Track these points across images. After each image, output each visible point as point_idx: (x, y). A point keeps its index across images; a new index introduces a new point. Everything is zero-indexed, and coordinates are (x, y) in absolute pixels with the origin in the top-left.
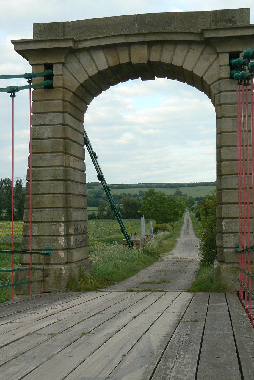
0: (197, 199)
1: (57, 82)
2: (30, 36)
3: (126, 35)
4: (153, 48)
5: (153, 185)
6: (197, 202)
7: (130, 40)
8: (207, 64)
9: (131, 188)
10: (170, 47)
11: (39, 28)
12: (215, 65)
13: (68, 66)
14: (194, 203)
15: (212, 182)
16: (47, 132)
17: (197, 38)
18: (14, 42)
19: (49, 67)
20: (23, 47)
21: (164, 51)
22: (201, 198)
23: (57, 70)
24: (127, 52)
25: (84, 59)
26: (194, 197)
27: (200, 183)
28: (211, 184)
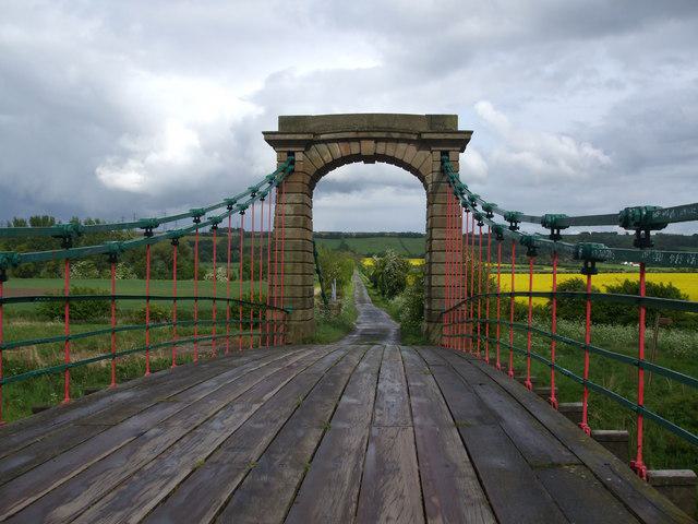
2: (275, 128)
7: (361, 135)
18: (264, 133)
20: (272, 137)
23: (299, 156)
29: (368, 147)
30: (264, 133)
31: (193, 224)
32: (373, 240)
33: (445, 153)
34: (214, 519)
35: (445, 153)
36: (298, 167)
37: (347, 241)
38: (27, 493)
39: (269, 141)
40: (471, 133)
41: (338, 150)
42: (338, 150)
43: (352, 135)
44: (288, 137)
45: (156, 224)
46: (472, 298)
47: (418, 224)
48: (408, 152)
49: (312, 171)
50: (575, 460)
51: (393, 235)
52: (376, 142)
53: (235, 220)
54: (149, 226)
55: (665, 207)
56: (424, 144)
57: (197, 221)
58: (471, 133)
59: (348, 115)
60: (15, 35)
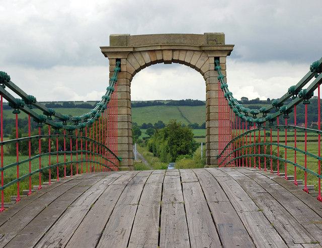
0: (144, 126)
1: (124, 69)
2: (108, 45)
3: (161, 46)
4: (175, 52)
5: (76, 104)
6: (145, 131)
7: (163, 48)
8: (203, 62)
9: (73, 107)
10: (184, 52)
11: (113, 39)
12: (207, 62)
13: (129, 60)
14: (140, 134)
15: (167, 101)
16: (124, 89)
17: (198, 49)
18: (101, 48)
19: (118, 60)
20: (106, 50)
21: (181, 54)
22: (150, 125)
23: (123, 62)
24: (161, 53)
25: (138, 56)
26: (140, 124)
27: (148, 101)
28: (165, 103)
29: (168, 56)
32: (149, 108)
33: (217, 58)
34: (43, 246)
35: (217, 58)
39: (103, 53)
40: (234, 46)
41: (147, 58)
44: (116, 50)
46: (193, 145)
48: (195, 59)
50: (266, 192)
51: (172, 103)
55: (107, 84)
56: (202, 50)
58: (234, 46)
59: (143, 35)
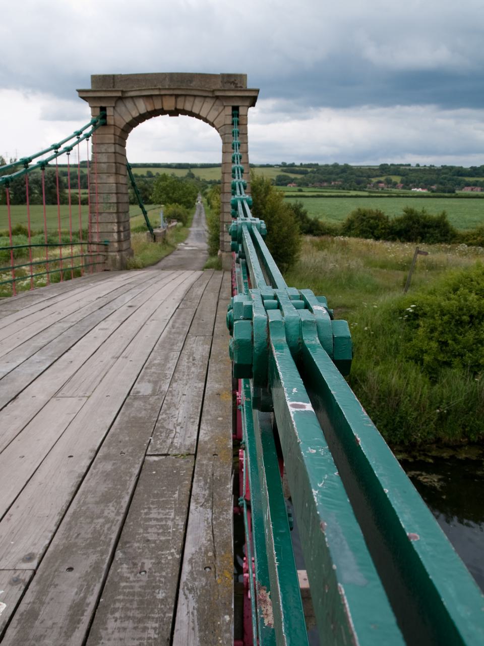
2: (88, 86)
7: (163, 92)
20: (85, 95)
23: (109, 112)
29: (169, 104)
30: (79, 91)
31: (77, 139)
33: (235, 109)
36: (110, 121)
37: (194, 171)
38: (258, 486)
40: (258, 91)
42: (142, 107)
43: (157, 92)
45: (30, 160)
47: (216, 157)
49: (122, 124)
52: (163, 109)
53: (62, 160)
54: (26, 162)
57: (78, 138)
60: (482, 596)
